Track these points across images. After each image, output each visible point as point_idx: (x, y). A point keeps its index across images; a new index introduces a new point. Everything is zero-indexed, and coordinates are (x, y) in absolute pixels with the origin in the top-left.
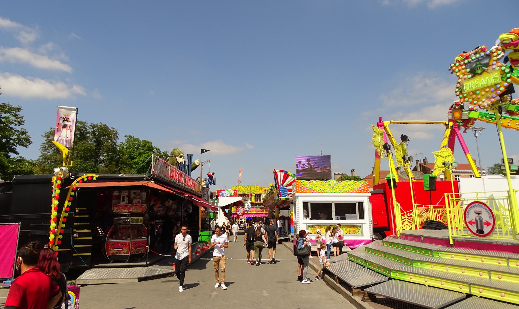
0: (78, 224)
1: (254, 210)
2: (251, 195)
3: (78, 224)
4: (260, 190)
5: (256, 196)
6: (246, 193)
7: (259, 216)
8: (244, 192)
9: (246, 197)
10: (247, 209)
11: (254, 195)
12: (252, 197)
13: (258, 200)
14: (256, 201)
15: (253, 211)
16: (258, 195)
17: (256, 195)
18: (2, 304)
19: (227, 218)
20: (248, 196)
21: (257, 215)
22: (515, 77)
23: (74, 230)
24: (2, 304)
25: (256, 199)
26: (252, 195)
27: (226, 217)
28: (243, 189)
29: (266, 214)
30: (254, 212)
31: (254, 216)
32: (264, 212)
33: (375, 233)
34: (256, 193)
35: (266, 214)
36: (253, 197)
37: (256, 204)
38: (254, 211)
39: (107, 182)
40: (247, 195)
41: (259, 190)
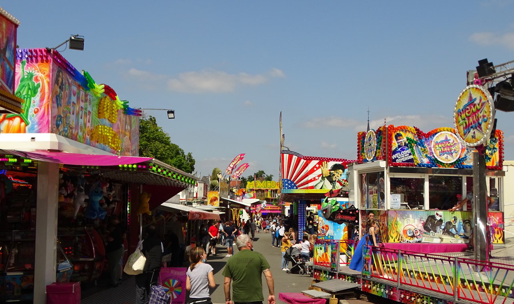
0: (94, 252)
1: (269, 207)
2: (267, 190)
3: (94, 252)
4: (276, 186)
5: (271, 192)
6: (262, 188)
7: (275, 212)
8: (260, 187)
9: (261, 192)
10: (264, 208)
11: (270, 190)
12: (267, 193)
13: (273, 196)
14: (271, 196)
15: (268, 208)
16: (274, 191)
17: (271, 190)
18: (216, 208)
19: (248, 214)
20: (264, 192)
21: (271, 212)
22: (430, 279)
23: (86, 265)
24: (216, 208)
25: (271, 195)
26: (268, 191)
27: (247, 213)
28: (259, 185)
29: (280, 210)
30: (269, 209)
31: (269, 212)
32: (279, 209)
33: (430, 184)
34: (272, 188)
35: (280, 210)
36: (269, 193)
37: (272, 200)
38: (269, 207)
39: (101, 167)
40: (262, 190)
41: (275, 185)
